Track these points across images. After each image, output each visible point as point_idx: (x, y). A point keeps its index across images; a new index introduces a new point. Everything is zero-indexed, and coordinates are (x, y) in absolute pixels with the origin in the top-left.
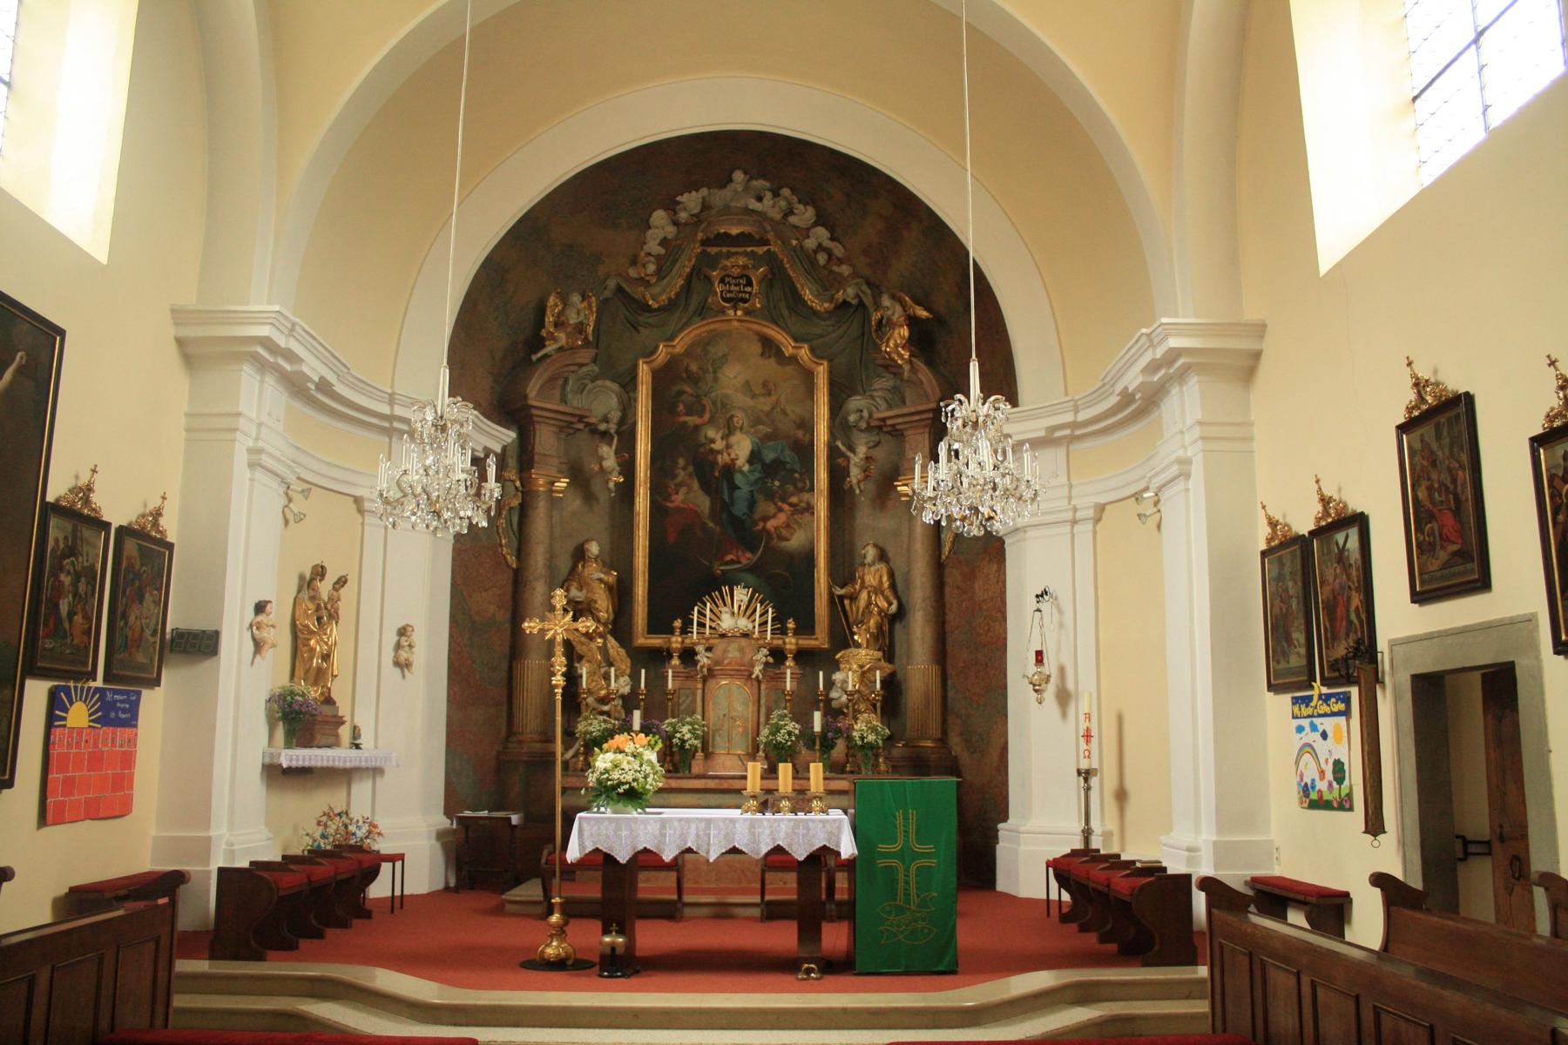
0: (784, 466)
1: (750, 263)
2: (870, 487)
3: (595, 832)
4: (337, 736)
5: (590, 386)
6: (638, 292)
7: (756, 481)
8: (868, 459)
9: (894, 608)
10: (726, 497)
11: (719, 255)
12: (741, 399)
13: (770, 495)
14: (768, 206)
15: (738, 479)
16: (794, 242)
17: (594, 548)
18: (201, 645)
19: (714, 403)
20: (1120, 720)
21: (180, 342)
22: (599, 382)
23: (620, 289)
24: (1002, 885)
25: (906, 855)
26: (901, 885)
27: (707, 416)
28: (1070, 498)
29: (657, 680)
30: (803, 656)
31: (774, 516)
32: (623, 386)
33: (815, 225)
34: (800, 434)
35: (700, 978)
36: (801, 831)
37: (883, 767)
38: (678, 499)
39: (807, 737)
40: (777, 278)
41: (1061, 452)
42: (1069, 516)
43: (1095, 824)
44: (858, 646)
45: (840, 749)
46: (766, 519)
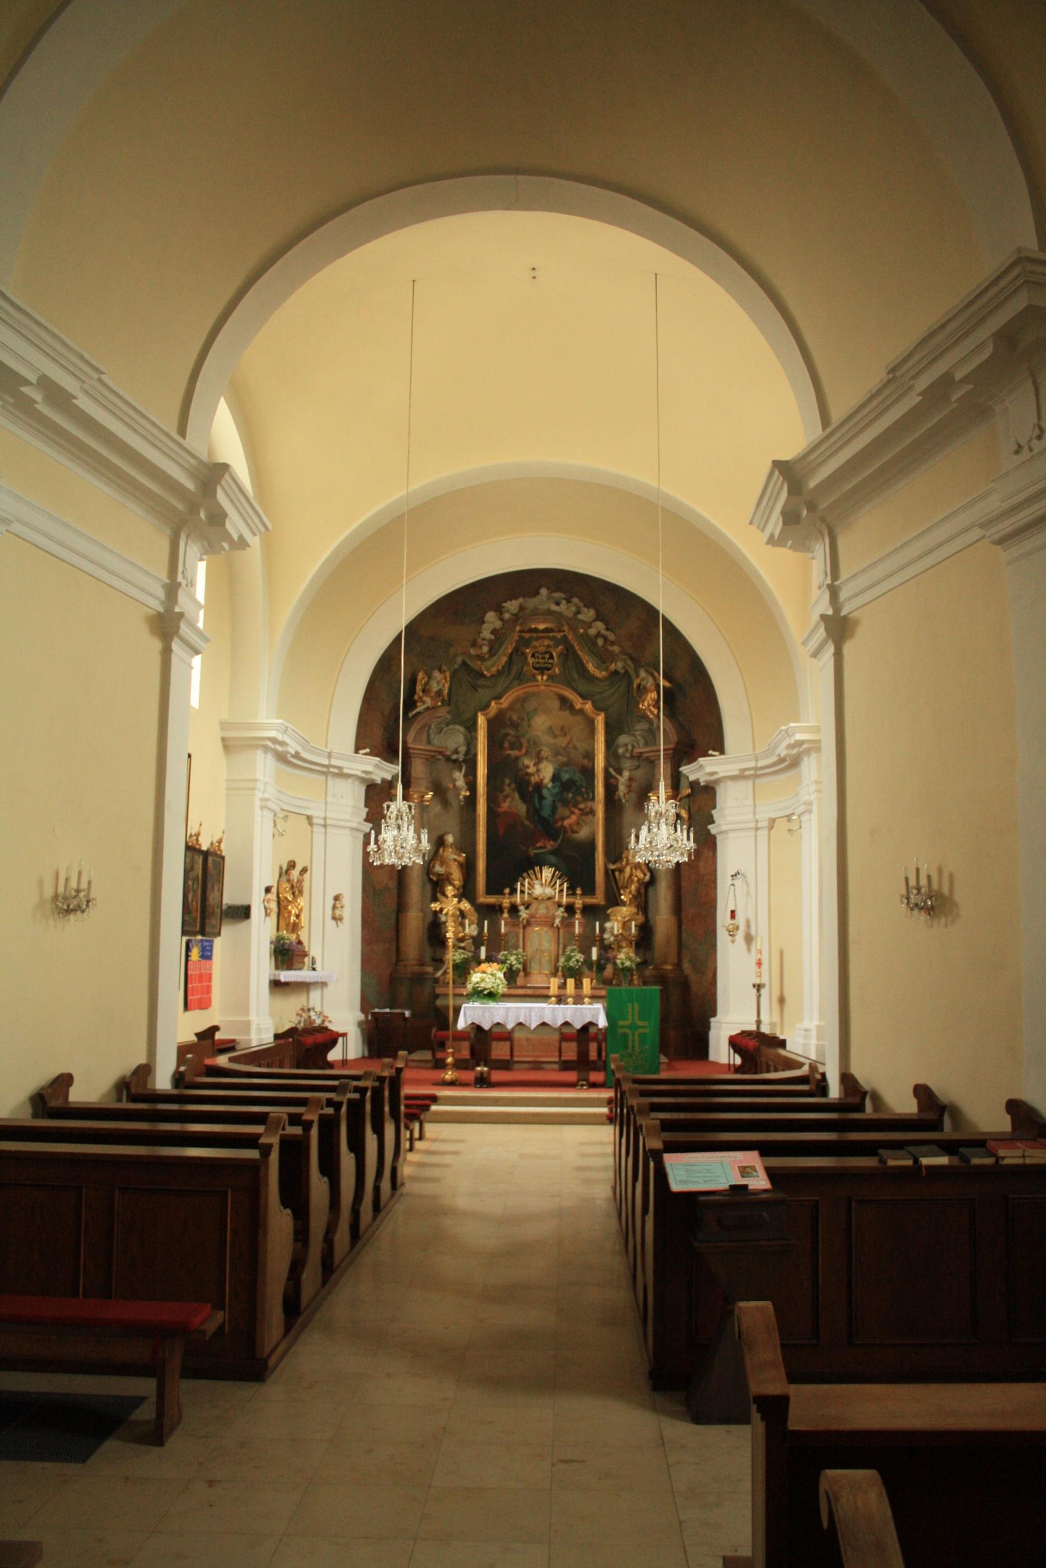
0: (575, 784)
1: (551, 643)
2: (633, 796)
3: (471, 1014)
4: (304, 963)
5: (445, 729)
6: (476, 665)
7: (557, 794)
8: (630, 779)
9: (647, 878)
10: (537, 805)
11: (530, 639)
12: (547, 739)
13: (566, 803)
14: (563, 607)
15: (545, 792)
16: (581, 631)
17: (450, 839)
18: (243, 913)
19: (529, 741)
20: (782, 953)
21: (223, 739)
22: (451, 727)
23: (464, 663)
24: (712, 1057)
25: (633, 1027)
26: (630, 1043)
27: (524, 751)
28: (755, 813)
29: (494, 927)
30: (587, 910)
31: (568, 817)
32: (467, 728)
33: (595, 620)
34: (586, 762)
35: (526, 1089)
36: (578, 1014)
37: (636, 982)
38: (505, 806)
39: (588, 962)
40: (569, 653)
41: (750, 783)
42: (753, 825)
43: (762, 1018)
44: (623, 904)
45: (609, 970)
46: (563, 819)
